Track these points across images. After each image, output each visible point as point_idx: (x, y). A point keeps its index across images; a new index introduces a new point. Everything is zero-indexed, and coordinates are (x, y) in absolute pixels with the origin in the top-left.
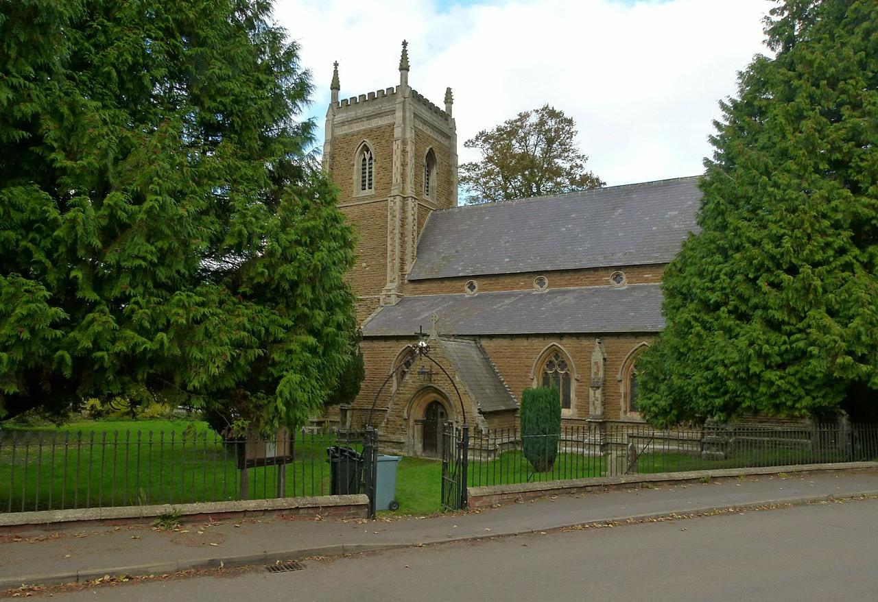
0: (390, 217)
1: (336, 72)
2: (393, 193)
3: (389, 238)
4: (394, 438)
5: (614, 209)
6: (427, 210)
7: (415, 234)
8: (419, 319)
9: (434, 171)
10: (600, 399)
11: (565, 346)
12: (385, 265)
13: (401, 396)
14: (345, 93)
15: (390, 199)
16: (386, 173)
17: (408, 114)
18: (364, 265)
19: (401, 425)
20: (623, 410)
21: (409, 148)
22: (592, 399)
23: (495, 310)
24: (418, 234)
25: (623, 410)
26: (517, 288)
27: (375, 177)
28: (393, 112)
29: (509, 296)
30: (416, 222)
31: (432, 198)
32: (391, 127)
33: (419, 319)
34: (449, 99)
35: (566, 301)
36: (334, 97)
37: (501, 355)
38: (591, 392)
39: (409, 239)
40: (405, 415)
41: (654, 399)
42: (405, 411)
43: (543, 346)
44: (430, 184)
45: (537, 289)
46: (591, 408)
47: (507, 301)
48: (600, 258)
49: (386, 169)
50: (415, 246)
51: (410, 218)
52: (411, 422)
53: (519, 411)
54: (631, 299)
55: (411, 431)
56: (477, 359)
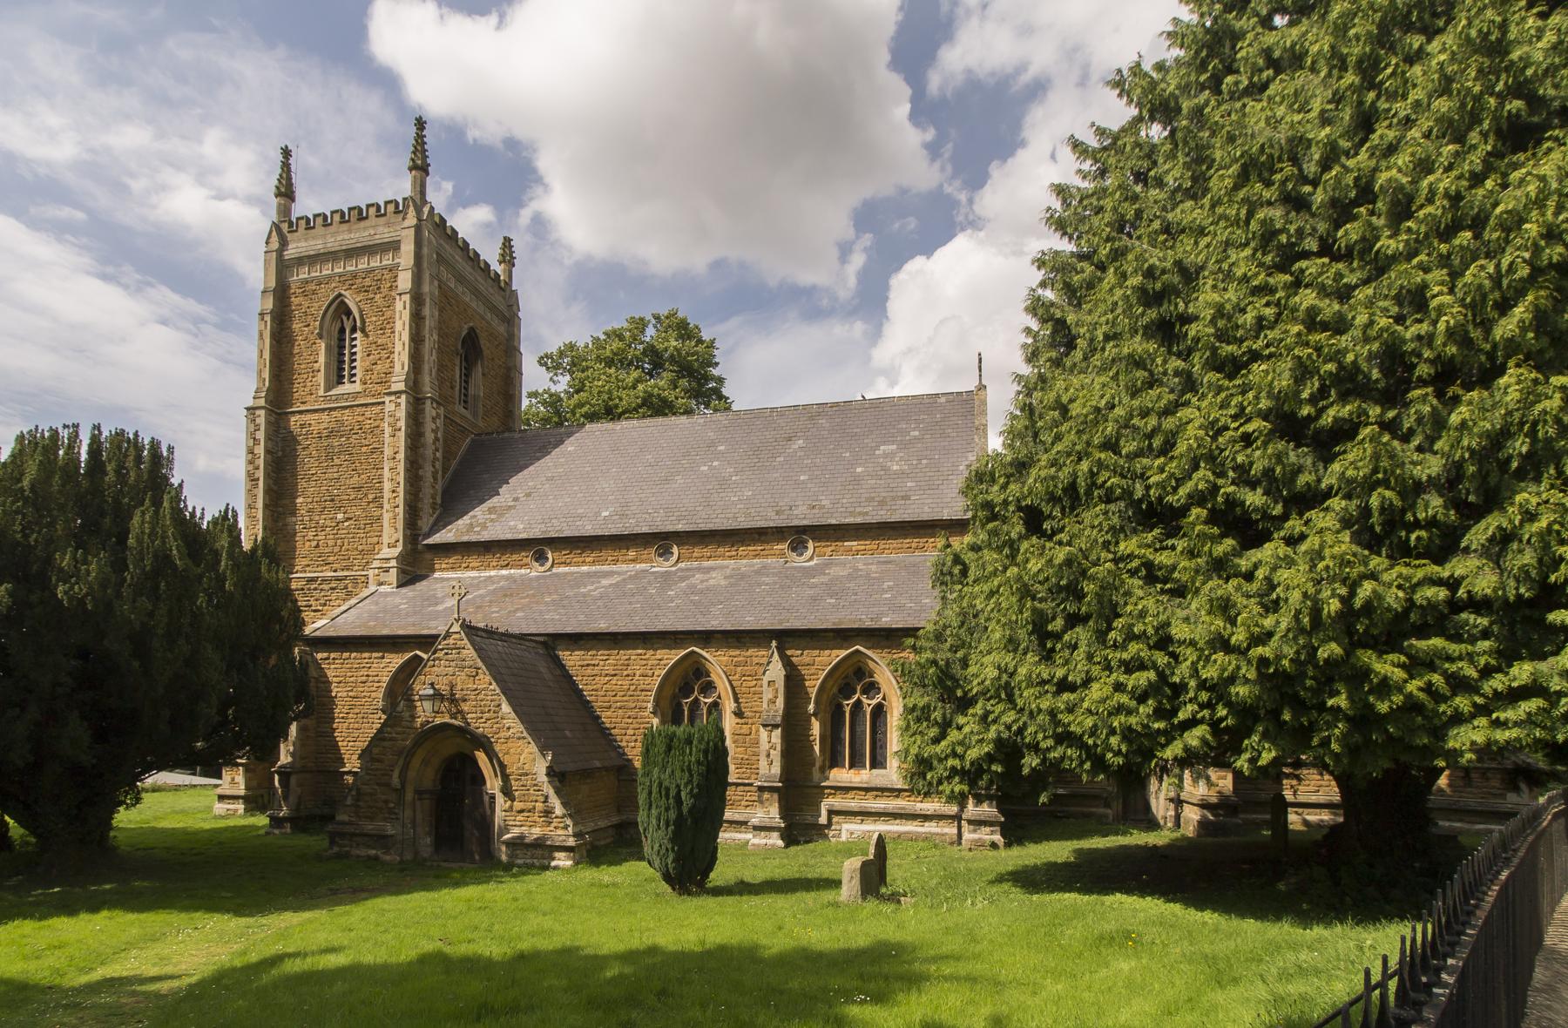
0: (388, 431)
1: (286, 166)
2: (395, 388)
3: (386, 469)
4: (369, 827)
5: (790, 439)
6: (464, 431)
7: (438, 465)
8: (440, 608)
9: (478, 371)
10: (779, 747)
11: (717, 662)
12: (379, 518)
13: (386, 744)
14: (306, 205)
15: (387, 399)
16: (384, 354)
17: (425, 251)
18: (340, 516)
19: (386, 802)
20: (818, 765)
21: (426, 311)
22: (764, 746)
23: (584, 596)
24: (445, 470)
25: (818, 765)
26: (624, 562)
27: (363, 360)
28: (394, 246)
29: (611, 573)
30: (440, 445)
31: (475, 414)
32: (393, 269)
33: (440, 608)
34: (508, 255)
35: (712, 582)
36: (285, 212)
37: (596, 670)
38: (764, 734)
39: (427, 471)
40: (395, 781)
41: (966, 729)
42: (396, 774)
43: (672, 656)
44: (471, 391)
45: (661, 566)
46: (763, 763)
47: (605, 582)
48: (772, 515)
49: (383, 347)
50: (439, 487)
51: (429, 437)
52: (409, 796)
53: (1282, 534)
54: (824, 579)
55: (408, 813)
56: (547, 676)
